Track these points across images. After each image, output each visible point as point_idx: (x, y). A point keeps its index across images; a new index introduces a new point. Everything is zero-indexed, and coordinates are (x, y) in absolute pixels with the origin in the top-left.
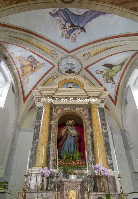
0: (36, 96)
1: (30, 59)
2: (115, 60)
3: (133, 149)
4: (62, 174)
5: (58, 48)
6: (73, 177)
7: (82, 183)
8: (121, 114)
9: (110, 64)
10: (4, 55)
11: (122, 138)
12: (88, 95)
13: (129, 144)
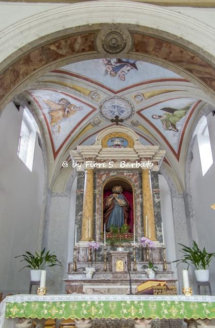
0: (75, 158)
1: (61, 103)
2: (177, 103)
3: (194, 217)
4: (109, 247)
5: (100, 88)
6: (120, 249)
7: (129, 254)
8: (185, 172)
9: (171, 107)
10: (27, 100)
11: (183, 202)
12: (139, 156)
13: (190, 211)
